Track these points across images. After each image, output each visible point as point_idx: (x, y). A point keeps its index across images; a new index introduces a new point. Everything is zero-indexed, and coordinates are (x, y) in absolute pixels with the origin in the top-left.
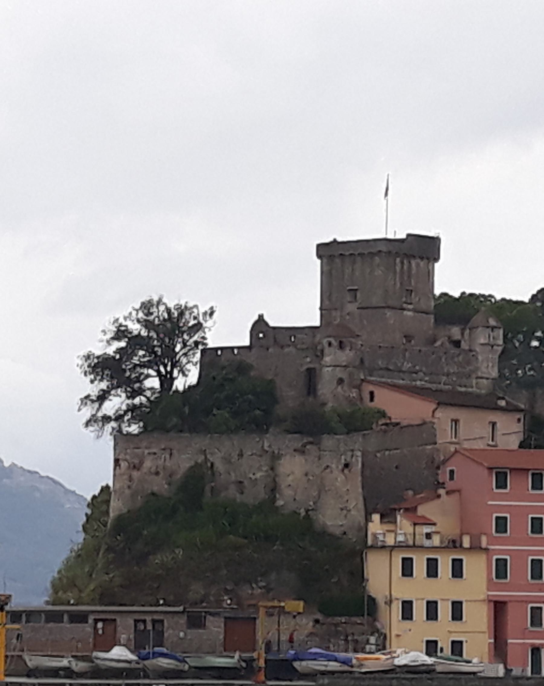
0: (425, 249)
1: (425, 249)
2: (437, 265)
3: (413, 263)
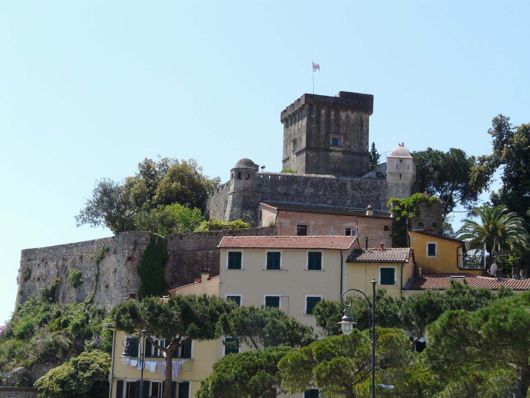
0: (362, 104)
1: (362, 104)
2: (371, 117)
3: (343, 115)
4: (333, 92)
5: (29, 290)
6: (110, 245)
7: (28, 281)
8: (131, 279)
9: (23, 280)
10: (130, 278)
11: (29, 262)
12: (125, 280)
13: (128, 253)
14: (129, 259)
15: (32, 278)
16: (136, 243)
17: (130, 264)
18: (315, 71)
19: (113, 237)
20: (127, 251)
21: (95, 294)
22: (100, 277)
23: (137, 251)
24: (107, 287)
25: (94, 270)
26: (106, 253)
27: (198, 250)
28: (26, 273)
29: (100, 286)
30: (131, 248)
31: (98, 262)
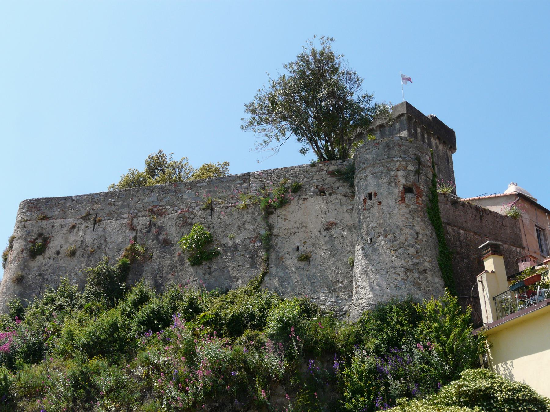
4: (427, 112)
5: (40, 275)
6: (302, 180)
7: (40, 258)
8: (421, 232)
9: (25, 255)
10: (417, 228)
11: (45, 222)
12: (406, 231)
13: (406, 177)
14: (408, 190)
15: (50, 251)
16: (418, 161)
17: (414, 201)
18: (406, 83)
19: (313, 165)
20: (401, 173)
21: (264, 274)
22: (279, 242)
23: (423, 178)
24: (306, 258)
25: (256, 226)
26: (290, 195)
27: (449, 224)
28: (34, 242)
29: (280, 259)
30: (411, 168)
31: (269, 211)
